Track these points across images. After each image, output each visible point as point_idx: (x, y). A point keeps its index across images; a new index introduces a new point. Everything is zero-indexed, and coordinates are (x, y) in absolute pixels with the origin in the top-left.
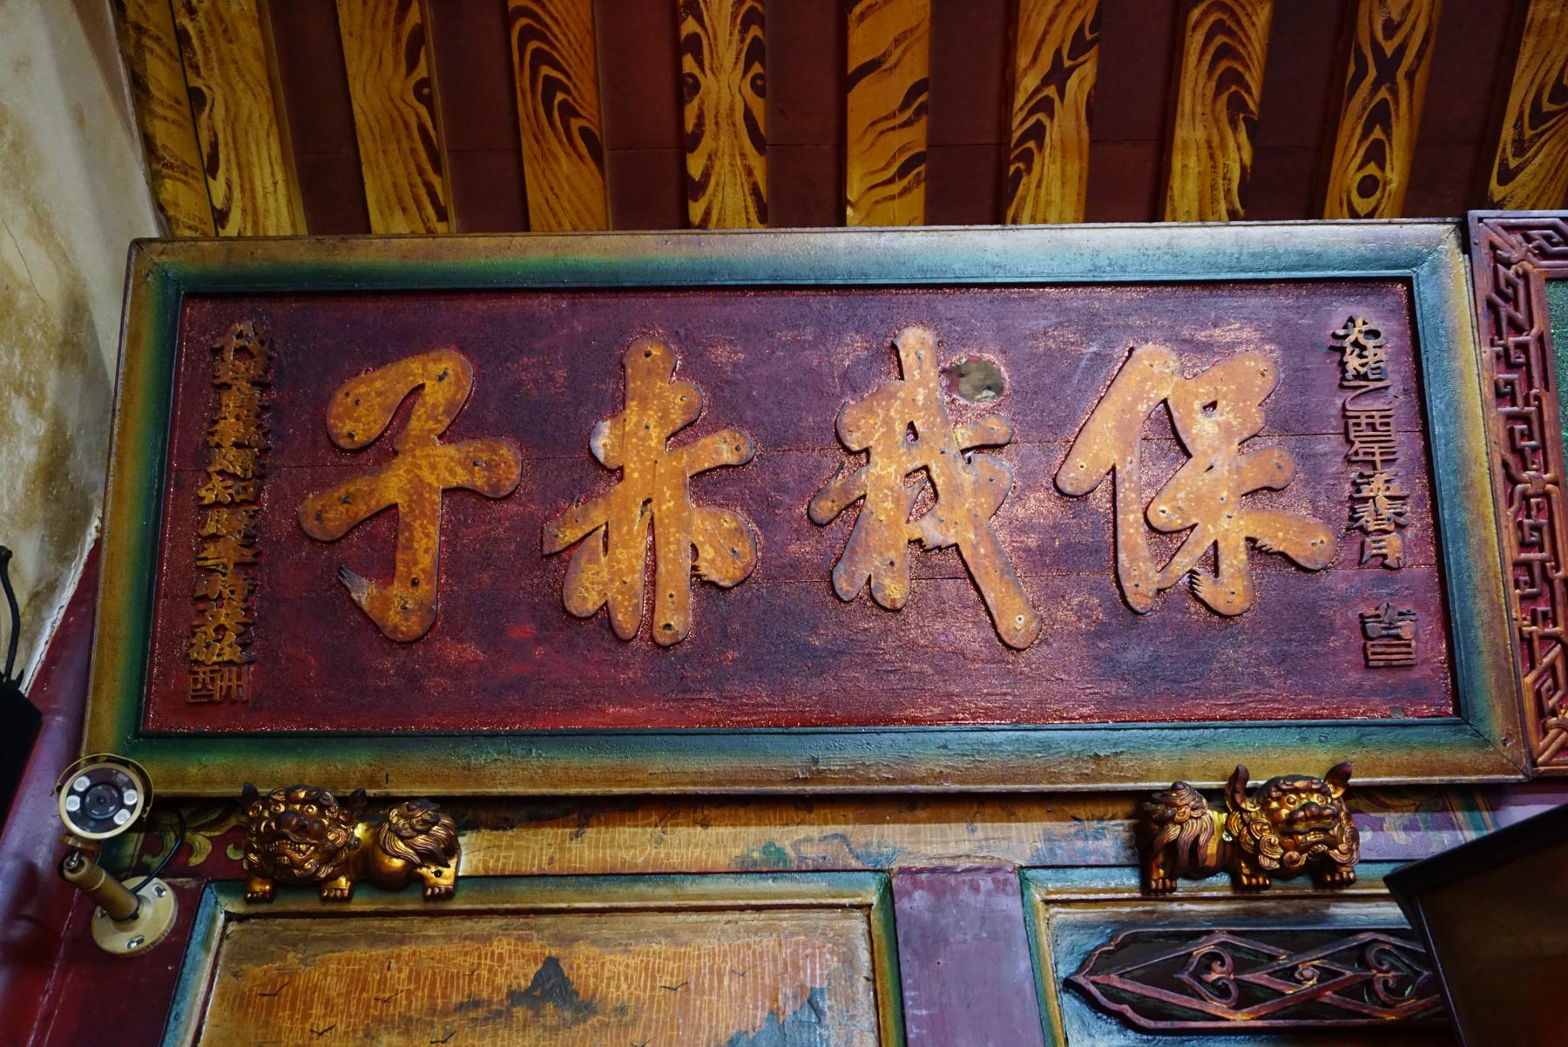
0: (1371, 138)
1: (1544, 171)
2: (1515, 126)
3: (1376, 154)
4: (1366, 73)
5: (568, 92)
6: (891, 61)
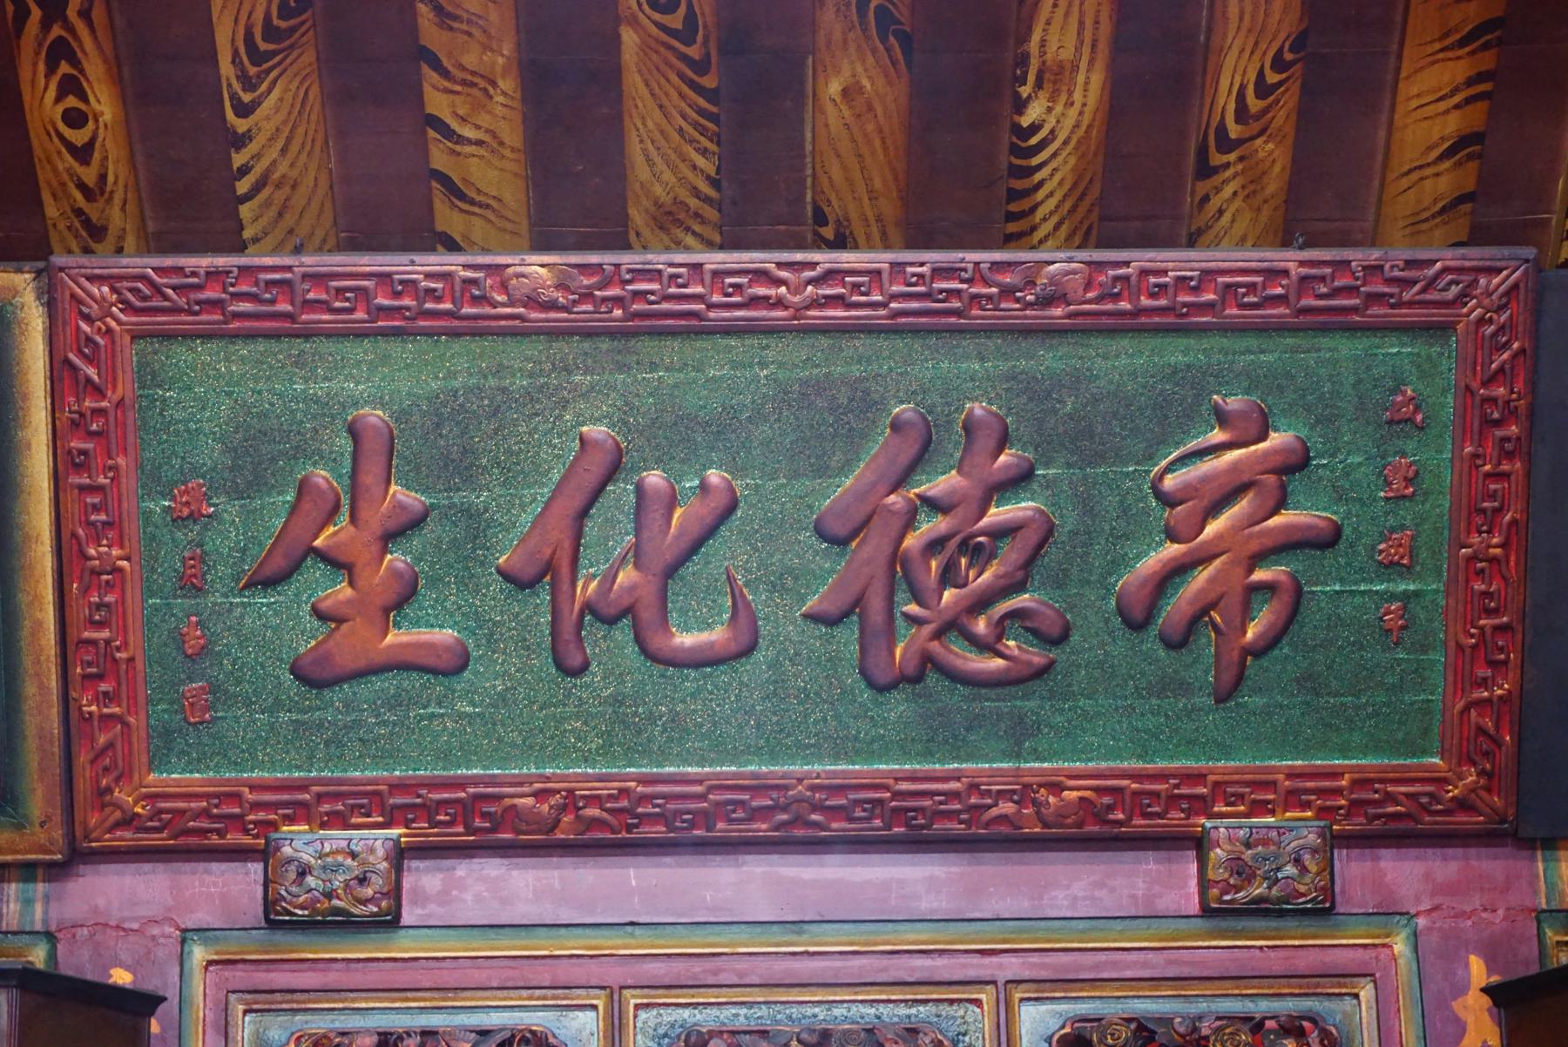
0: (60, 72)
1: (285, 110)
2: (233, 62)
3: (71, 86)
4: (29, 12)
5: (684, 58)
6: (456, 25)
